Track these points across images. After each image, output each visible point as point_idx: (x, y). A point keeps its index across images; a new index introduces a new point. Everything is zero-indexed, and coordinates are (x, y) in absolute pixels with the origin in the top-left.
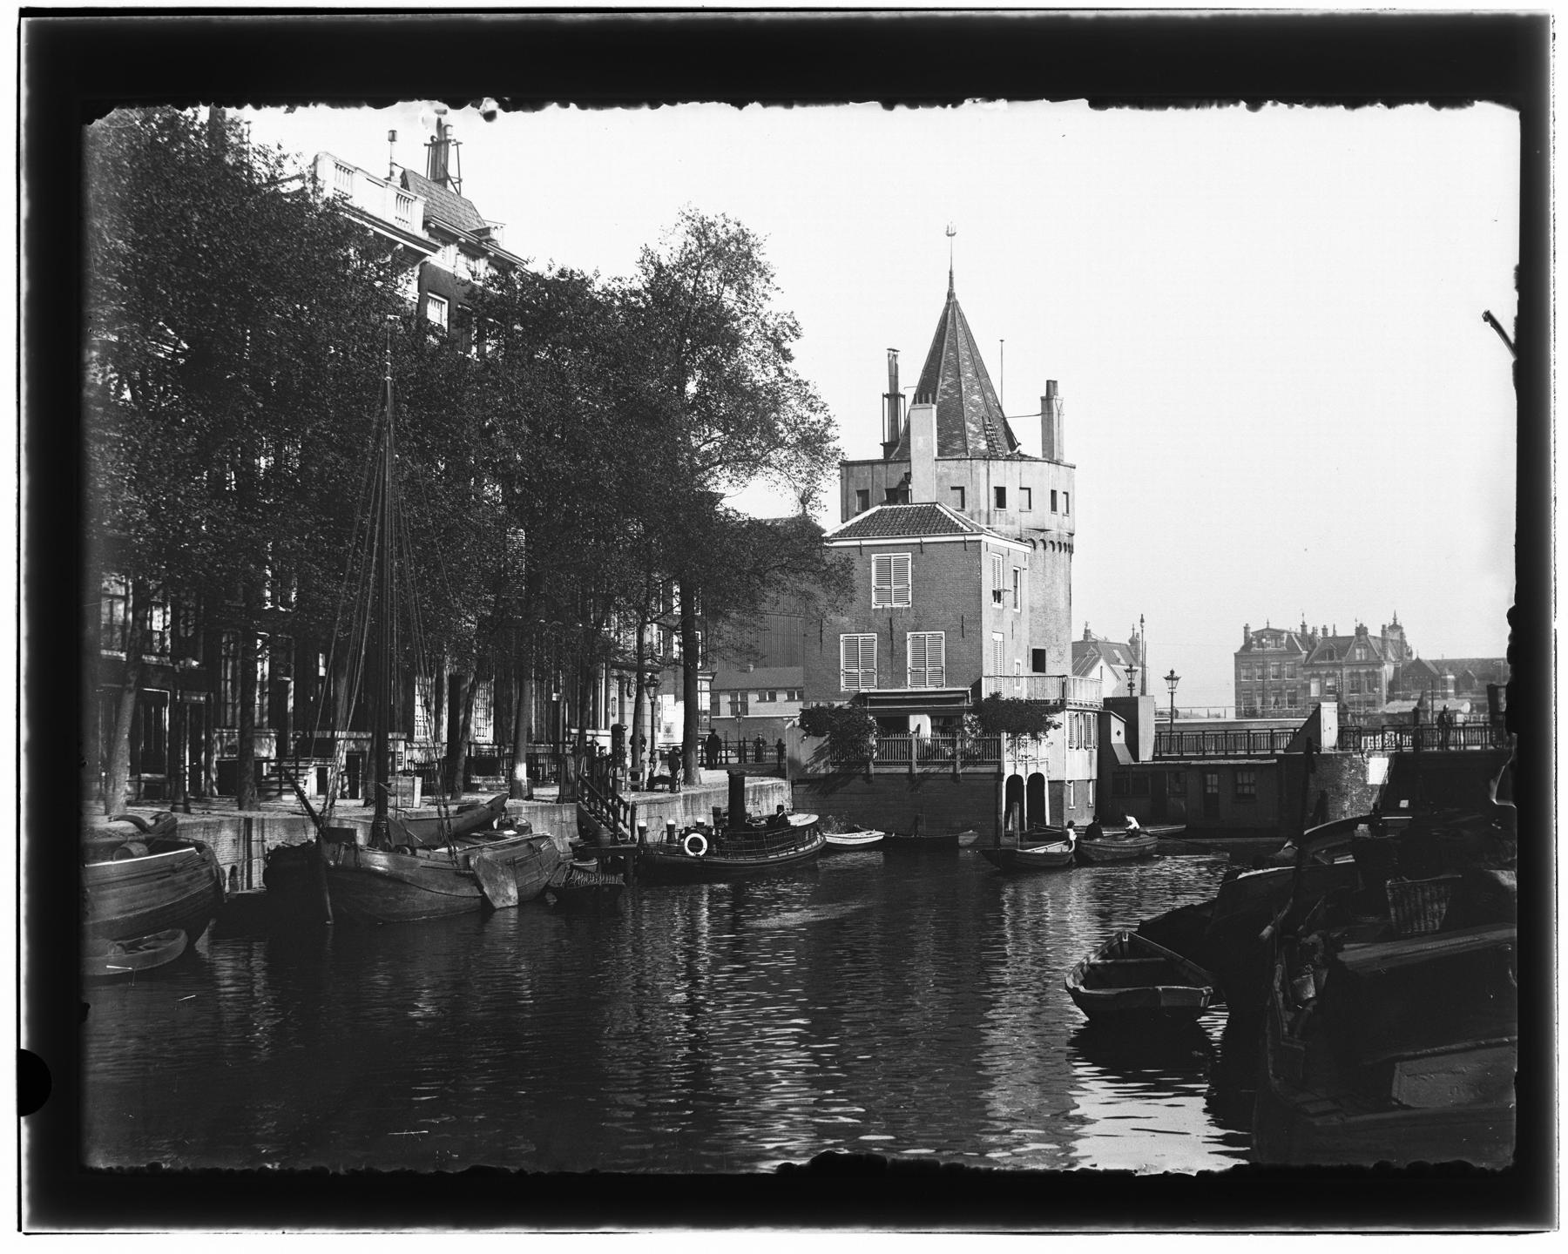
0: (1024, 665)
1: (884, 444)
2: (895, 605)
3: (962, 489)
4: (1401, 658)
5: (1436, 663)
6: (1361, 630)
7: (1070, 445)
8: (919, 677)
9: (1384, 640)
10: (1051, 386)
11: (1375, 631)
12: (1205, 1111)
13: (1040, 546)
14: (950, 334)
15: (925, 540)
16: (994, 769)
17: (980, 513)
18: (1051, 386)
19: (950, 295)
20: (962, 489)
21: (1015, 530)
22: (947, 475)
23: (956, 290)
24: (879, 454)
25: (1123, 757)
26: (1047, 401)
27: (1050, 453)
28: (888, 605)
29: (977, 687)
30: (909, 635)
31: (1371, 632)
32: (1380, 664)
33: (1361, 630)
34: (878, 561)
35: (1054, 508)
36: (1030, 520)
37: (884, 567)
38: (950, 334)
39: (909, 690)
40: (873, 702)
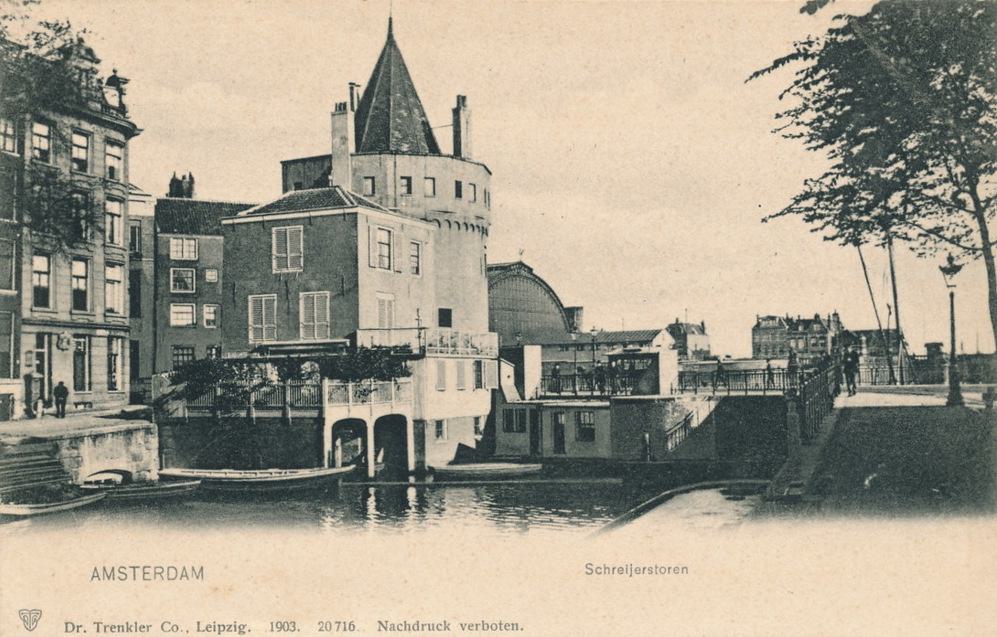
0: (430, 320)
1: (914, 355)
2: (291, 270)
3: (373, 178)
4: (838, 329)
5: (857, 332)
6: (817, 316)
7: (473, 146)
8: (309, 329)
9: (829, 320)
10: (462, 100)
11: (824, 317)
12: (974, 218)
13: (445, 225)
14: (390, 62)
15: (313, 214)
16: (314, 414)
17: (387, 197)
18: (462, 100)
19: (390, 36)
20: (373, 178)
21: (421, 212)
22: (360, 168)
23: (394, 32)
24: (910, 353)
25: (511, 394)
26: (456, 112)
27: (457, 153)
28: (285, 271)
29: (353, 337)
30: (301, 294)
31: (821, 317)
32: (827, 332)
33: (817, 316)
34: (278, 232)
35: (459, 194)
36: (435, 204)
37: (282, 236)
38: (390, 62)
39: (302, 341)
40: (273, 353)
